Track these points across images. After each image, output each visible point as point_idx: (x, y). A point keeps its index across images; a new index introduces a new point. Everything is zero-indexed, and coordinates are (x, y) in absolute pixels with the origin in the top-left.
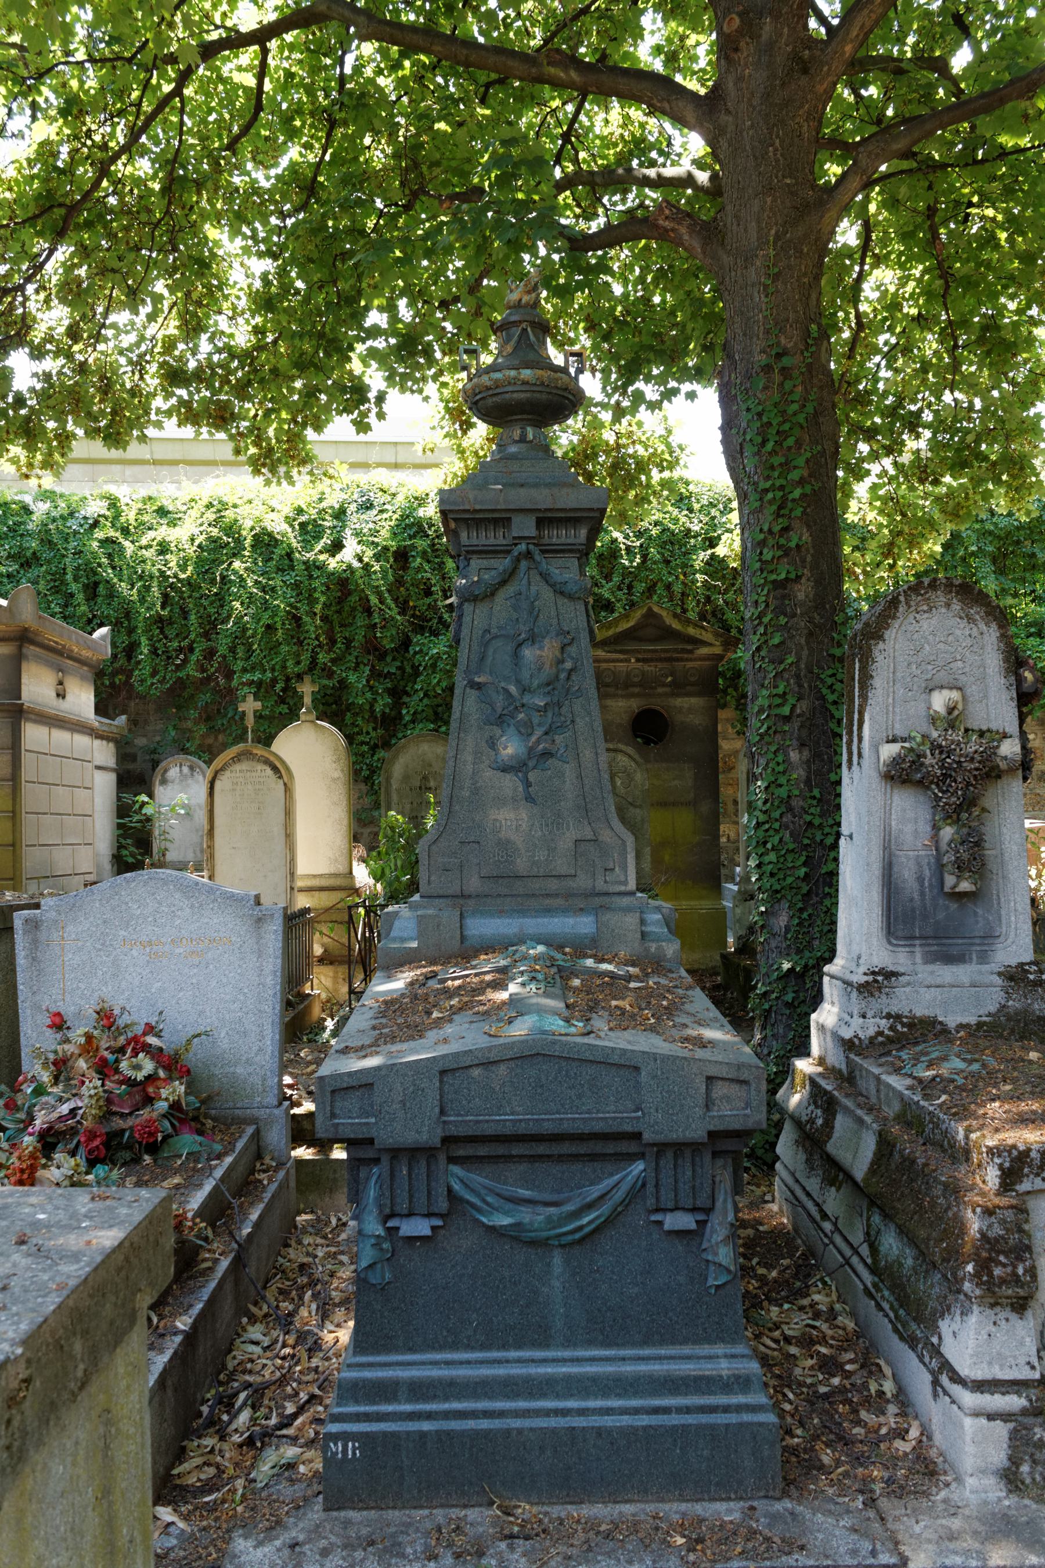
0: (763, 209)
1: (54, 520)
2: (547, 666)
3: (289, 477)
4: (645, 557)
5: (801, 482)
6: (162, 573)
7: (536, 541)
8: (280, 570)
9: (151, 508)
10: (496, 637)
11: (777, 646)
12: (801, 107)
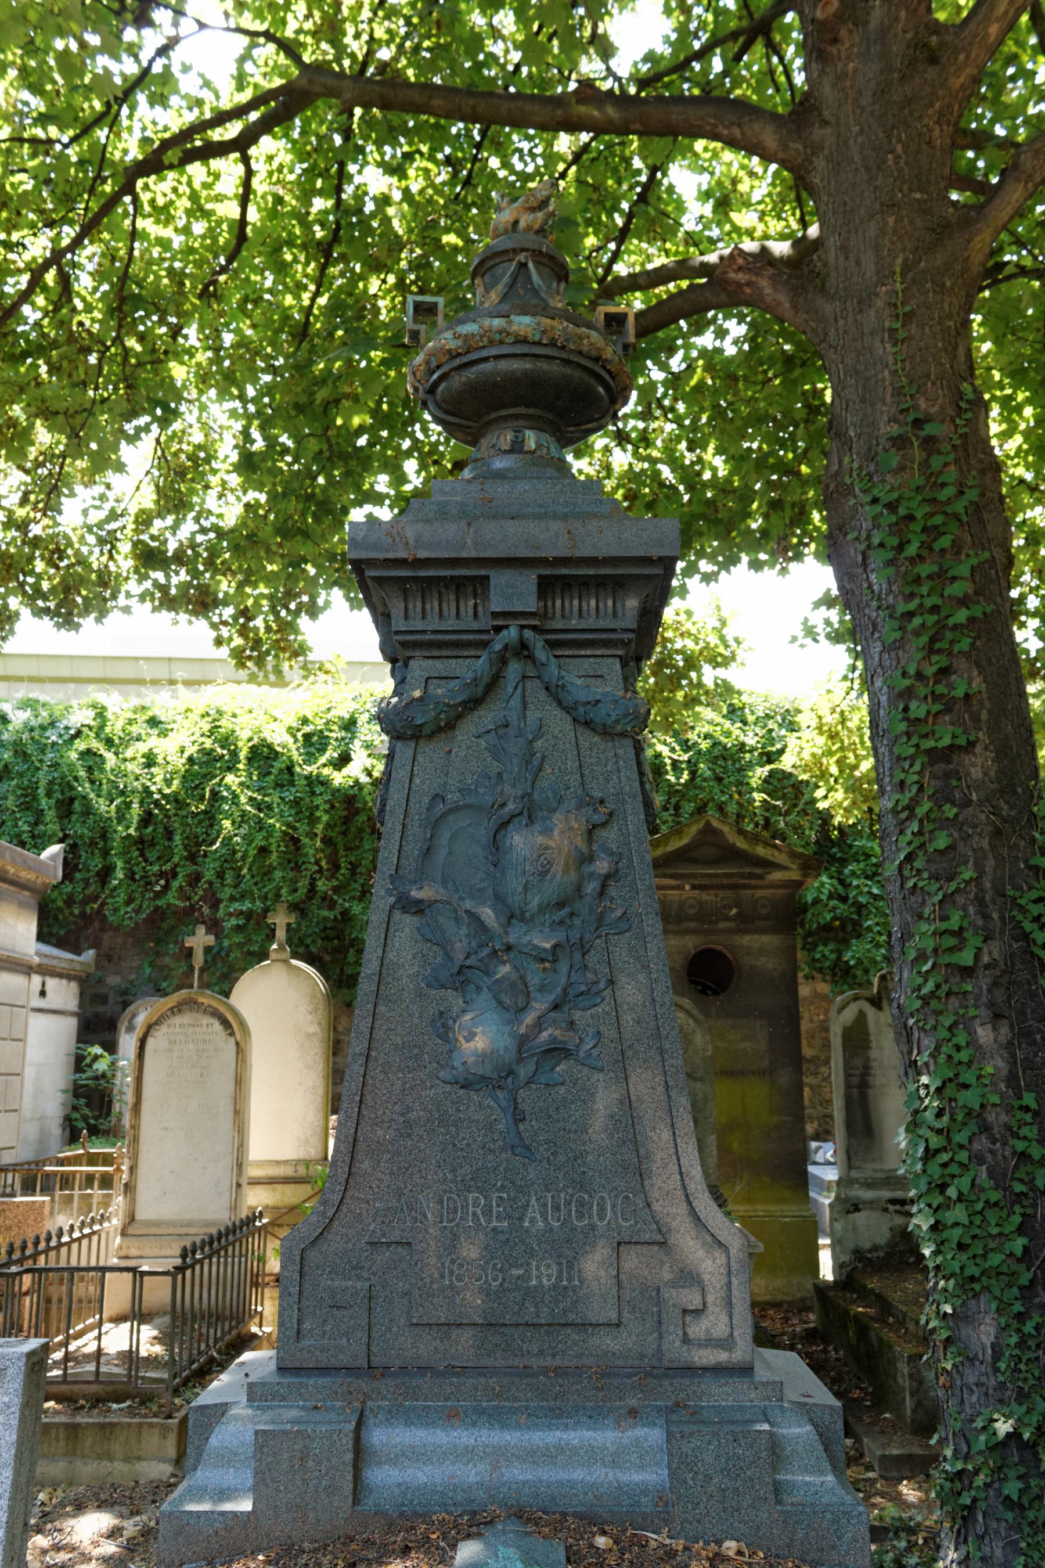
0: (883, 232)
1: (32, 730)
2: (558, 868)
3: (278, 671)
4: (693, 774)
5: (963, 602)
6: (147, 790)
7: (537, 622)
8: (278, 785)
9: (142, 718)
10: (456, 809)
11: (941, 852)
12: (931, 105)
